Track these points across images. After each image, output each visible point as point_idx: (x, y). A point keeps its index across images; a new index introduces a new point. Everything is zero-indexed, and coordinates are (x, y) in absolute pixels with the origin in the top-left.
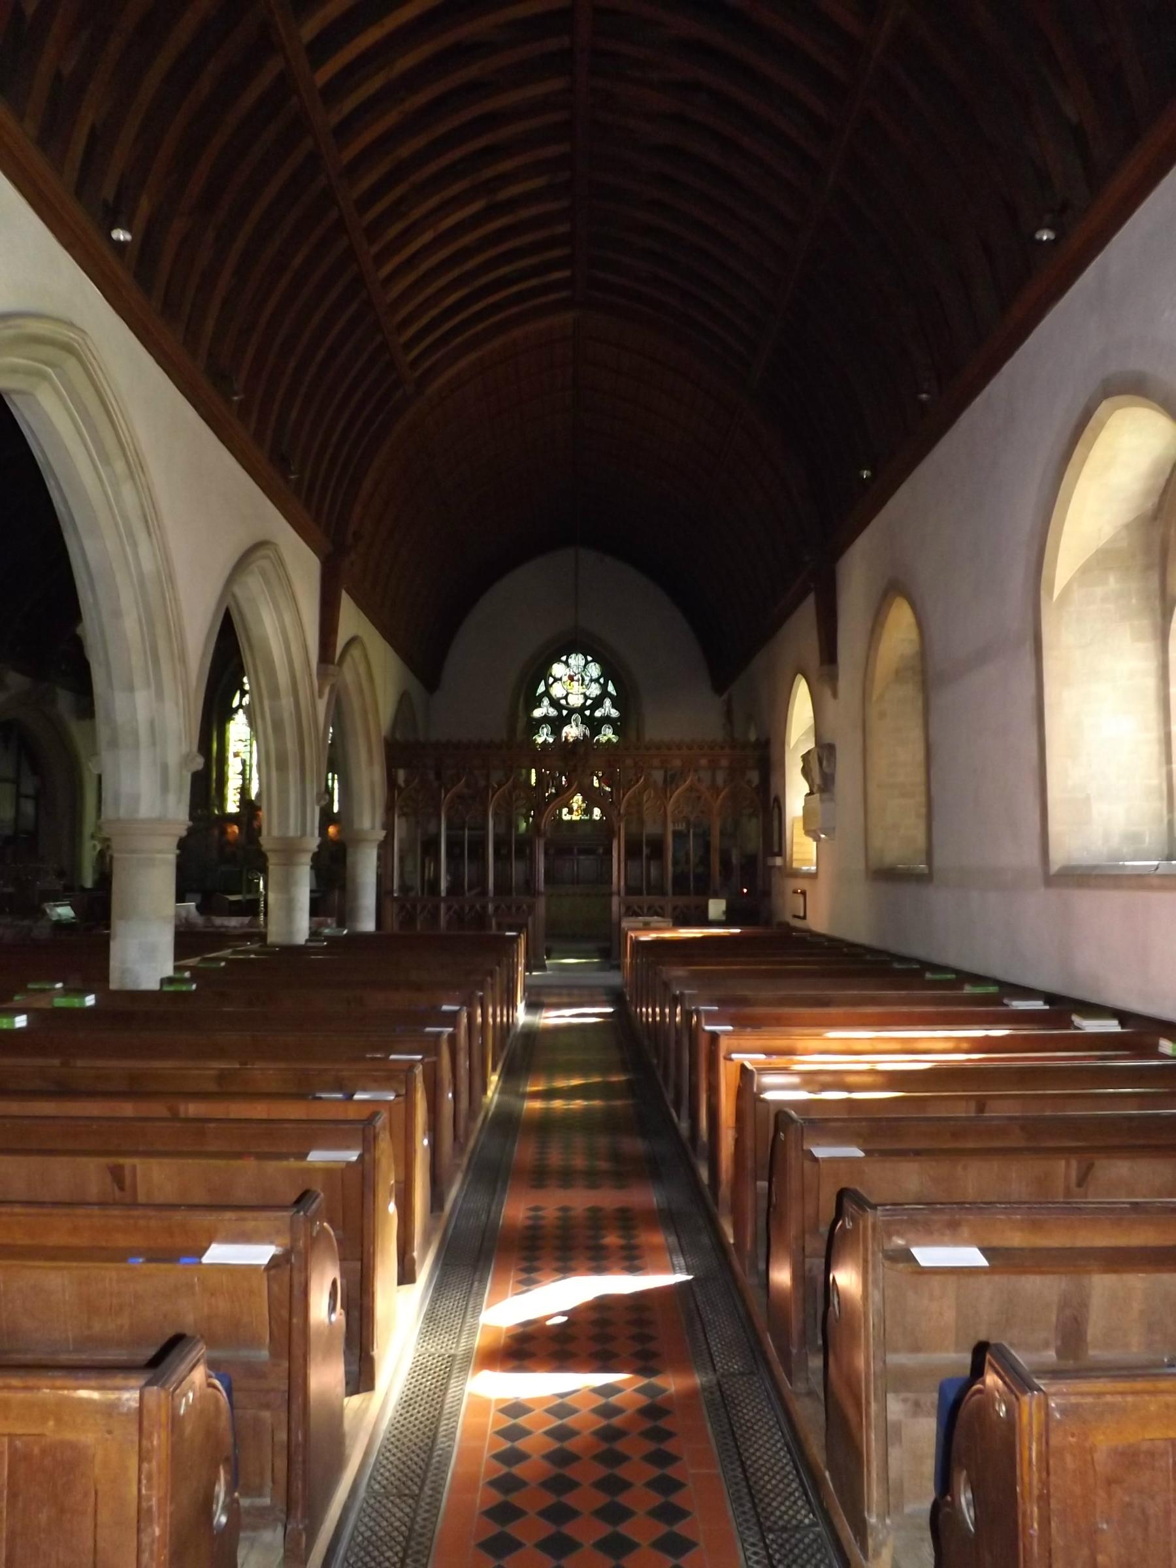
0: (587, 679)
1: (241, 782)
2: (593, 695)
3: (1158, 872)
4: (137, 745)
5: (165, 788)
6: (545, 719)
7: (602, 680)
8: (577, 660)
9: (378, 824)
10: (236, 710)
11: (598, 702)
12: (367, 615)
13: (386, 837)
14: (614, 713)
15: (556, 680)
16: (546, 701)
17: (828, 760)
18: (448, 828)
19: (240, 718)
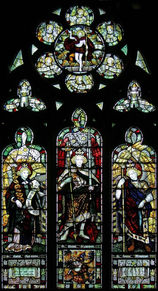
6: (24, 116)
11: (117, 88)
16: (25, 88)
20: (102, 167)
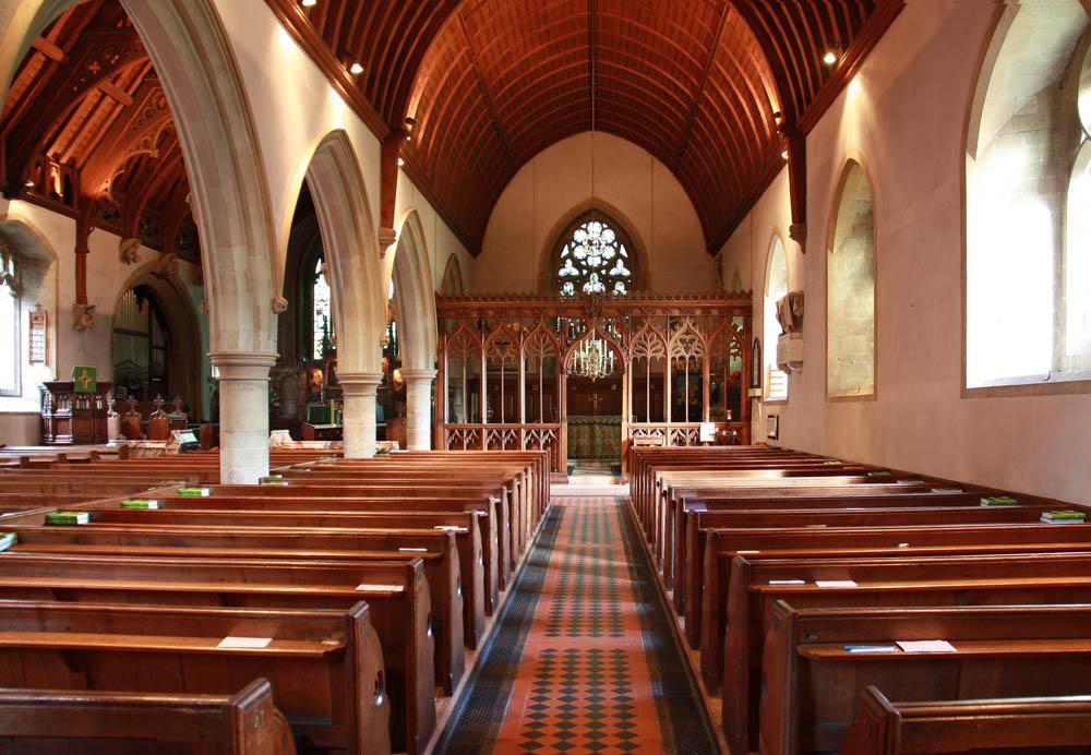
0: (603, 243)
1: (323, 334)
2: (608, 257)
3: (1049, 381)
4: (235, 292)
5: (257, 326)
6: (569, 278)
7: (615, 244)
8: (595, 227)
9: (432, 364)
10: (317, 276)
11: (612, 263)
12: (419, 188)
13: (437, 375)
14: (626, 273)
15: (578, 244)
16: (569, 262)
17: (798, 303)
18: (488, 370)
19: (321, 280)
20: (396, 161)
